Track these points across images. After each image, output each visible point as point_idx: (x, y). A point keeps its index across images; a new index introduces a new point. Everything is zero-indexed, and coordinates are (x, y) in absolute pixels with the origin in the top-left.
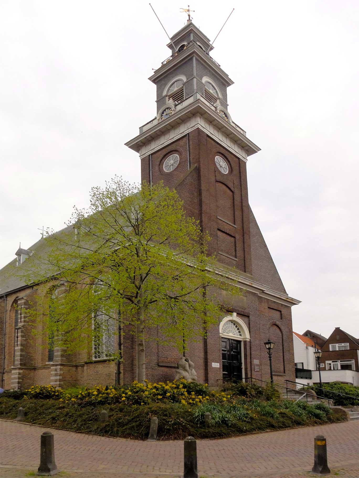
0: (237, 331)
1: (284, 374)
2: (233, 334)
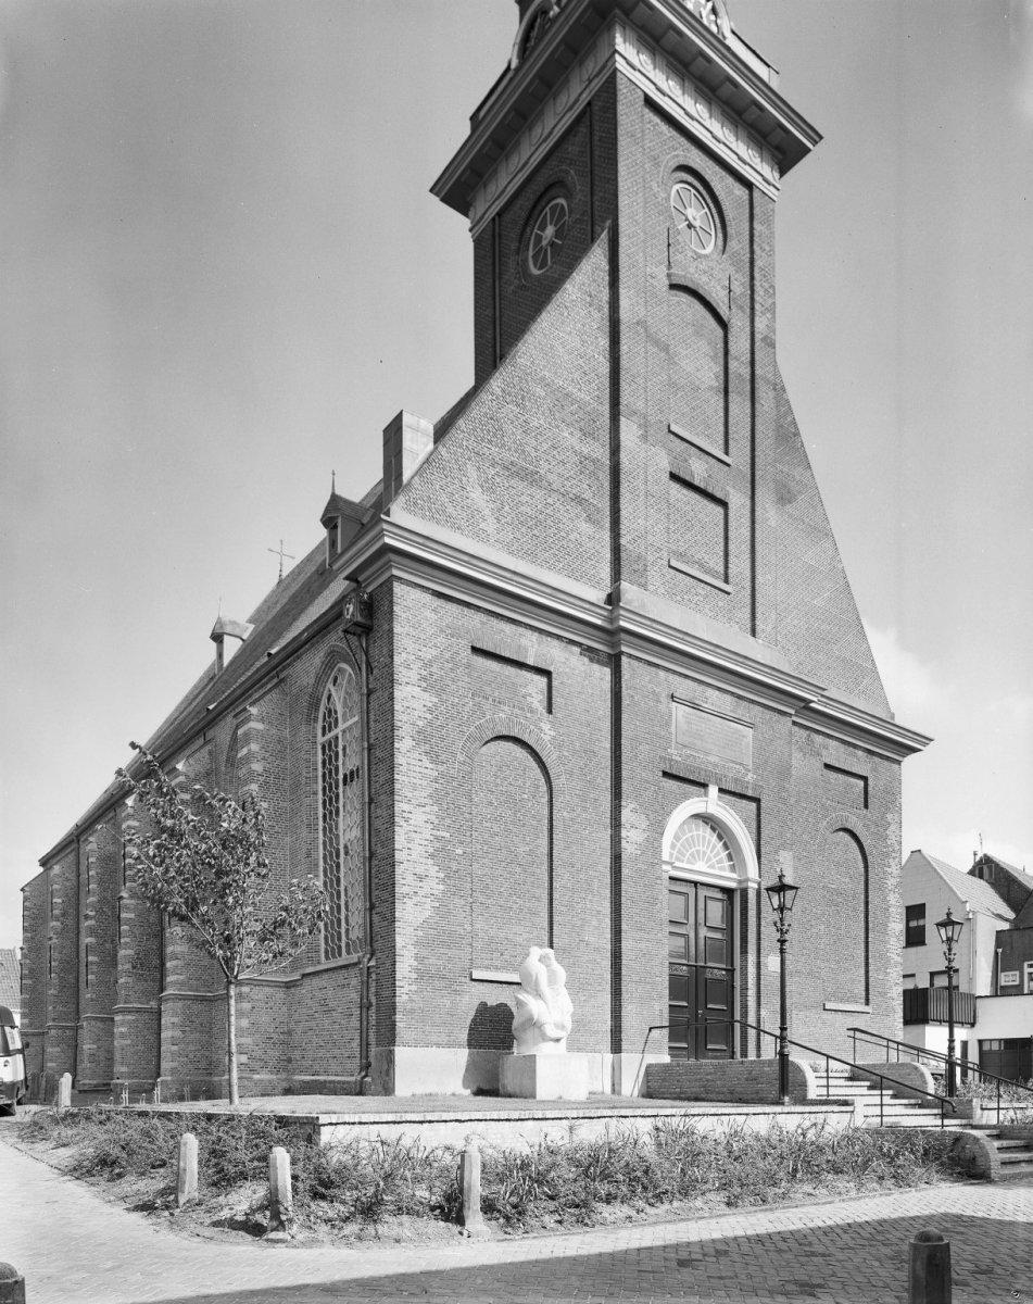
0: (724, 854)
1: (867, 1009)
2: (710, 865)
